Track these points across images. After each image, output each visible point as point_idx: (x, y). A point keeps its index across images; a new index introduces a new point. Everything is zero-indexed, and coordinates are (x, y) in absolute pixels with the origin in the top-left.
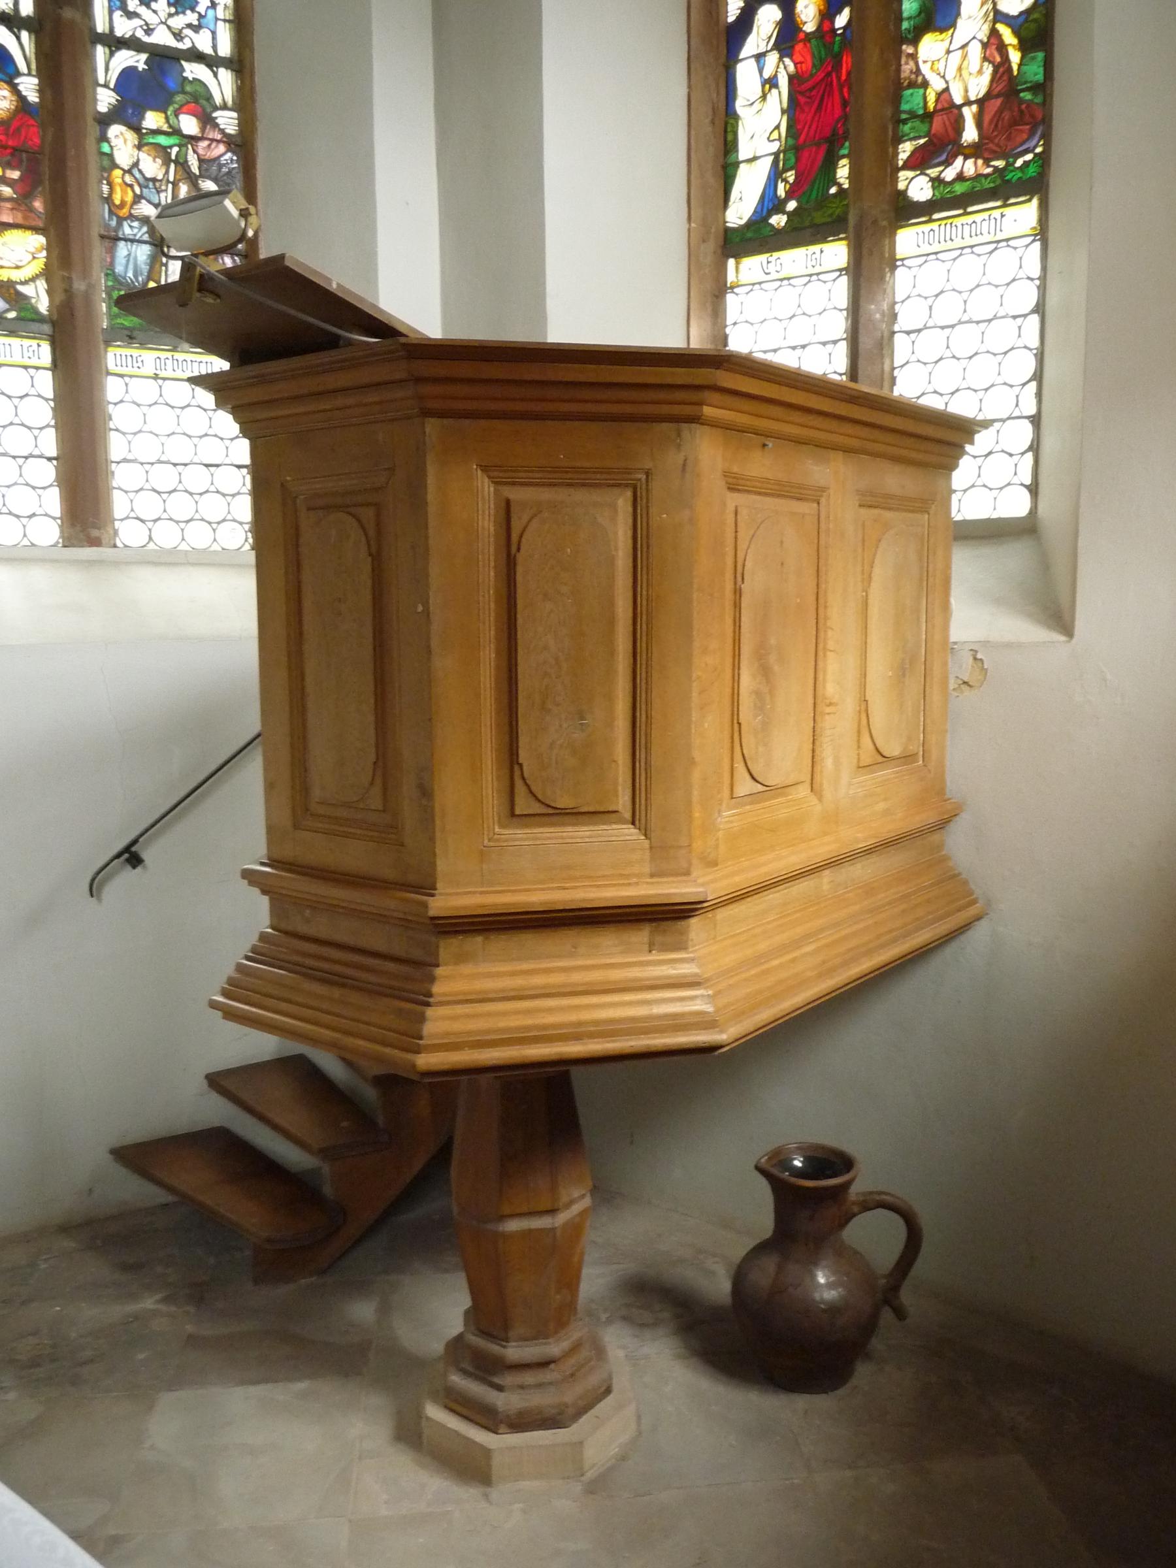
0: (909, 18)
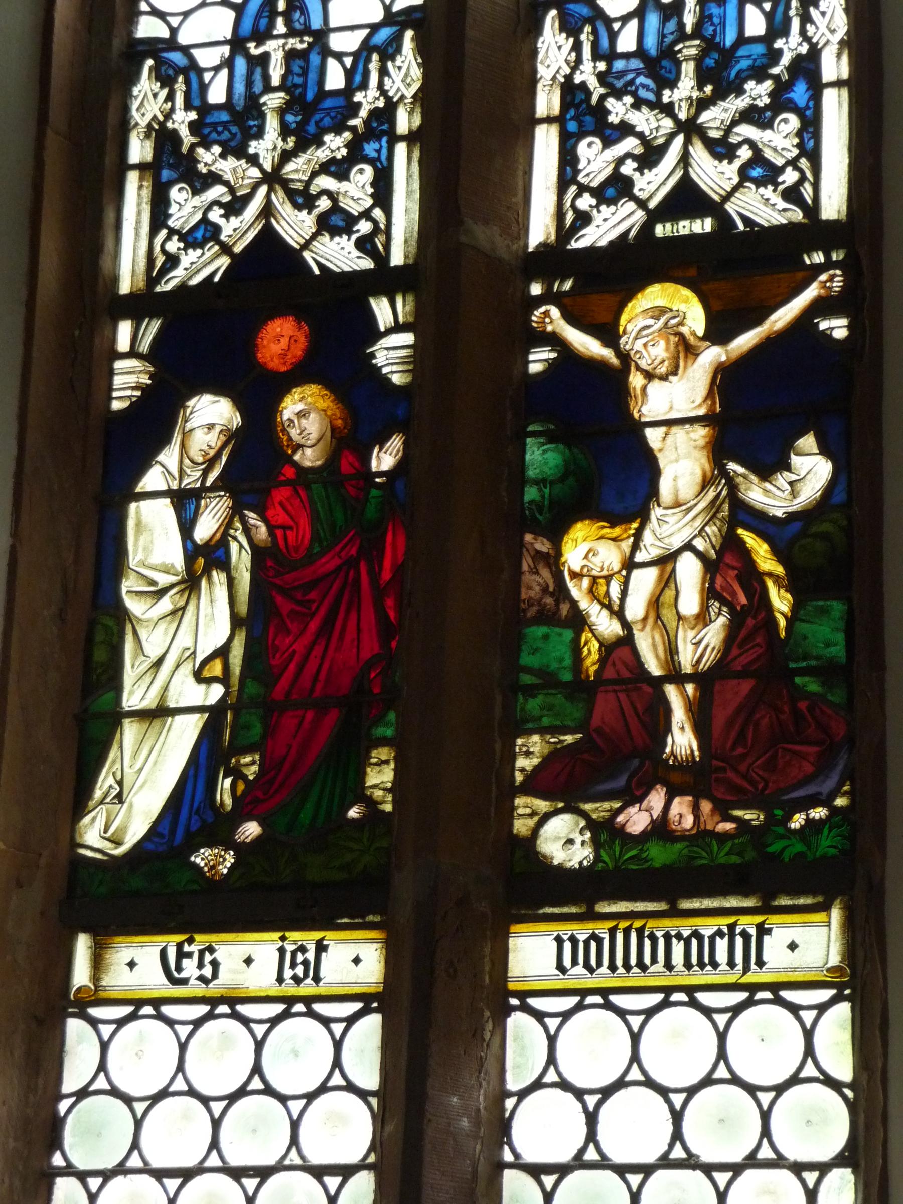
0: (540, 482)
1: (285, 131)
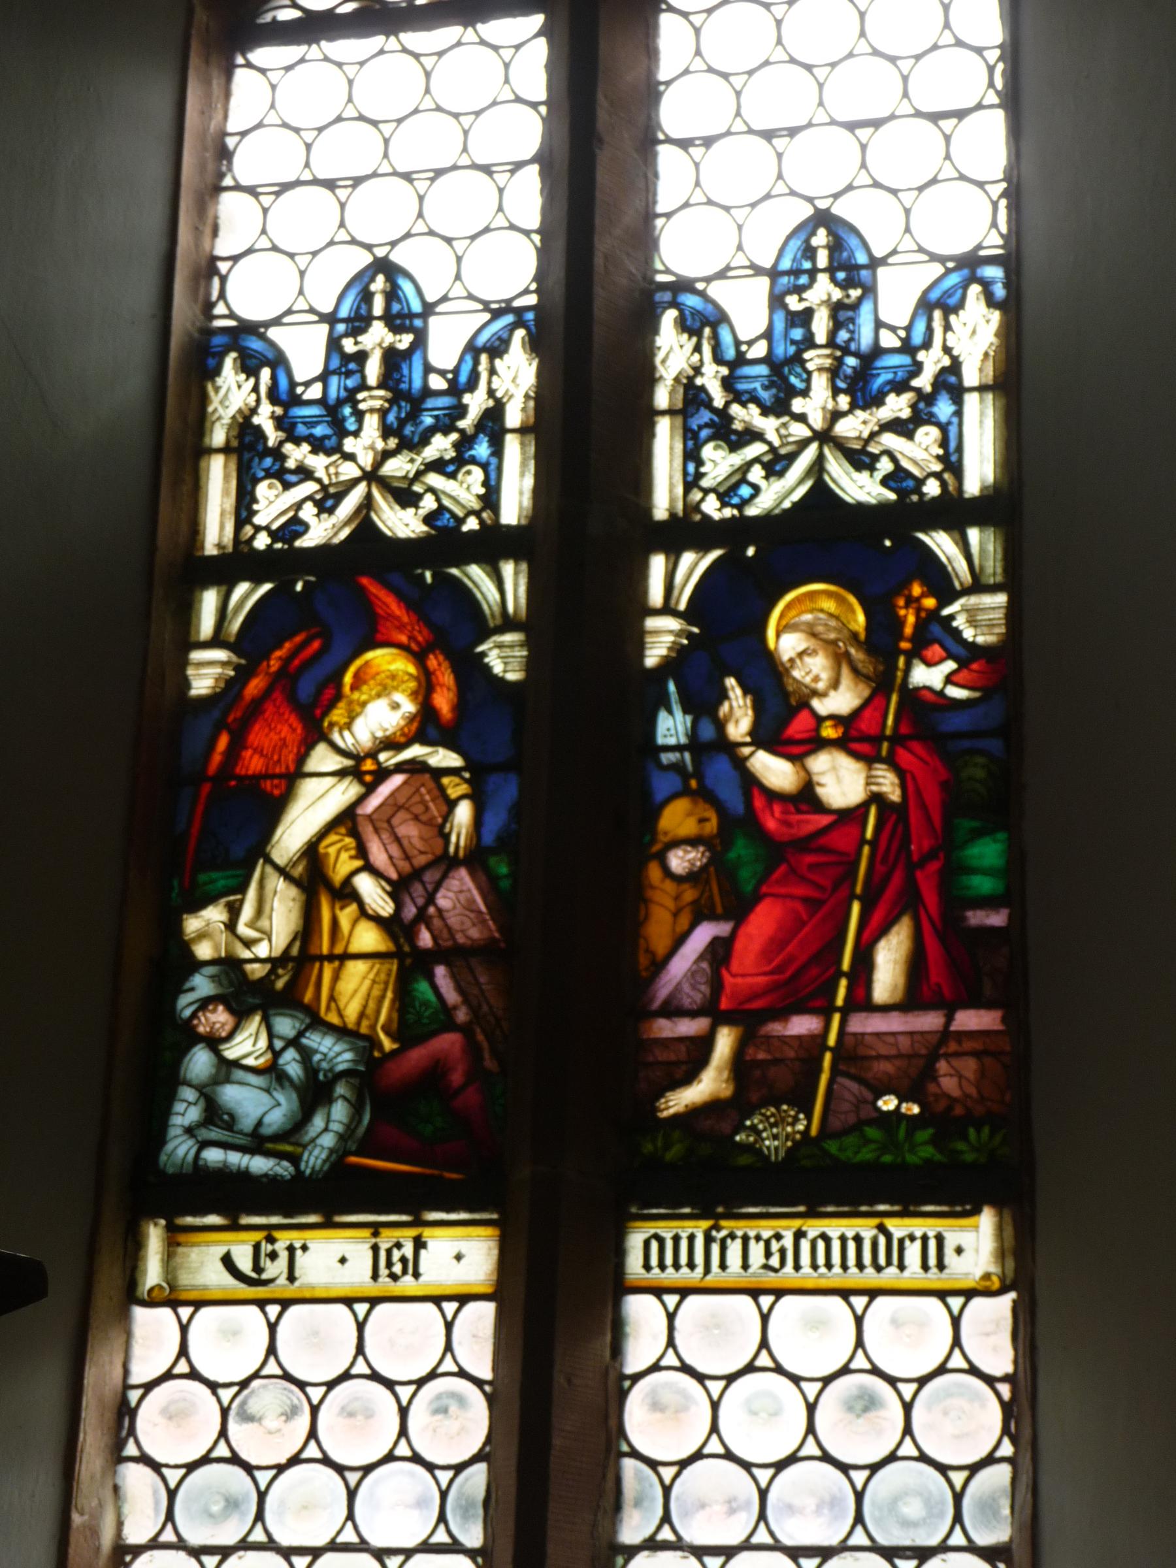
1: (386, 432)
